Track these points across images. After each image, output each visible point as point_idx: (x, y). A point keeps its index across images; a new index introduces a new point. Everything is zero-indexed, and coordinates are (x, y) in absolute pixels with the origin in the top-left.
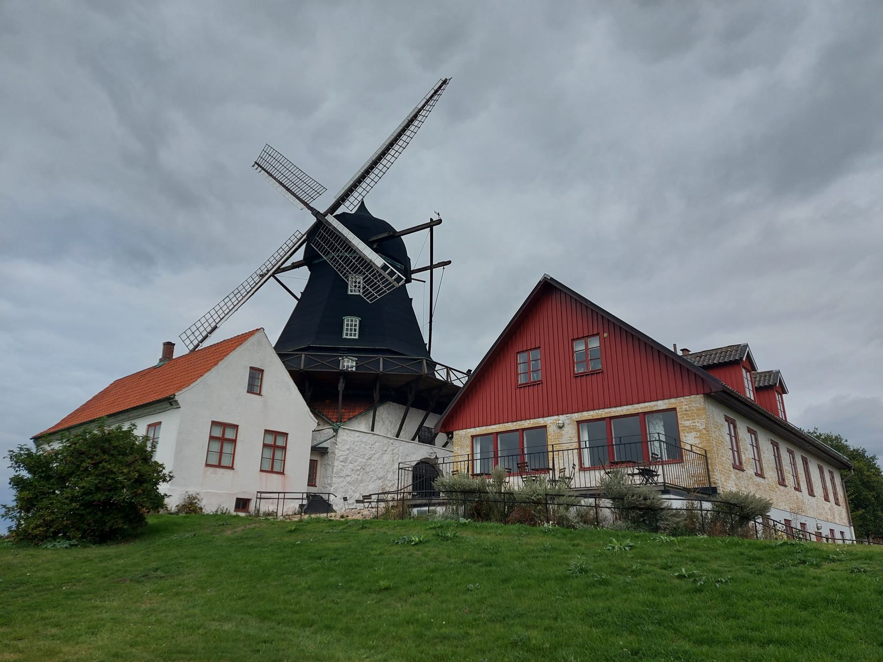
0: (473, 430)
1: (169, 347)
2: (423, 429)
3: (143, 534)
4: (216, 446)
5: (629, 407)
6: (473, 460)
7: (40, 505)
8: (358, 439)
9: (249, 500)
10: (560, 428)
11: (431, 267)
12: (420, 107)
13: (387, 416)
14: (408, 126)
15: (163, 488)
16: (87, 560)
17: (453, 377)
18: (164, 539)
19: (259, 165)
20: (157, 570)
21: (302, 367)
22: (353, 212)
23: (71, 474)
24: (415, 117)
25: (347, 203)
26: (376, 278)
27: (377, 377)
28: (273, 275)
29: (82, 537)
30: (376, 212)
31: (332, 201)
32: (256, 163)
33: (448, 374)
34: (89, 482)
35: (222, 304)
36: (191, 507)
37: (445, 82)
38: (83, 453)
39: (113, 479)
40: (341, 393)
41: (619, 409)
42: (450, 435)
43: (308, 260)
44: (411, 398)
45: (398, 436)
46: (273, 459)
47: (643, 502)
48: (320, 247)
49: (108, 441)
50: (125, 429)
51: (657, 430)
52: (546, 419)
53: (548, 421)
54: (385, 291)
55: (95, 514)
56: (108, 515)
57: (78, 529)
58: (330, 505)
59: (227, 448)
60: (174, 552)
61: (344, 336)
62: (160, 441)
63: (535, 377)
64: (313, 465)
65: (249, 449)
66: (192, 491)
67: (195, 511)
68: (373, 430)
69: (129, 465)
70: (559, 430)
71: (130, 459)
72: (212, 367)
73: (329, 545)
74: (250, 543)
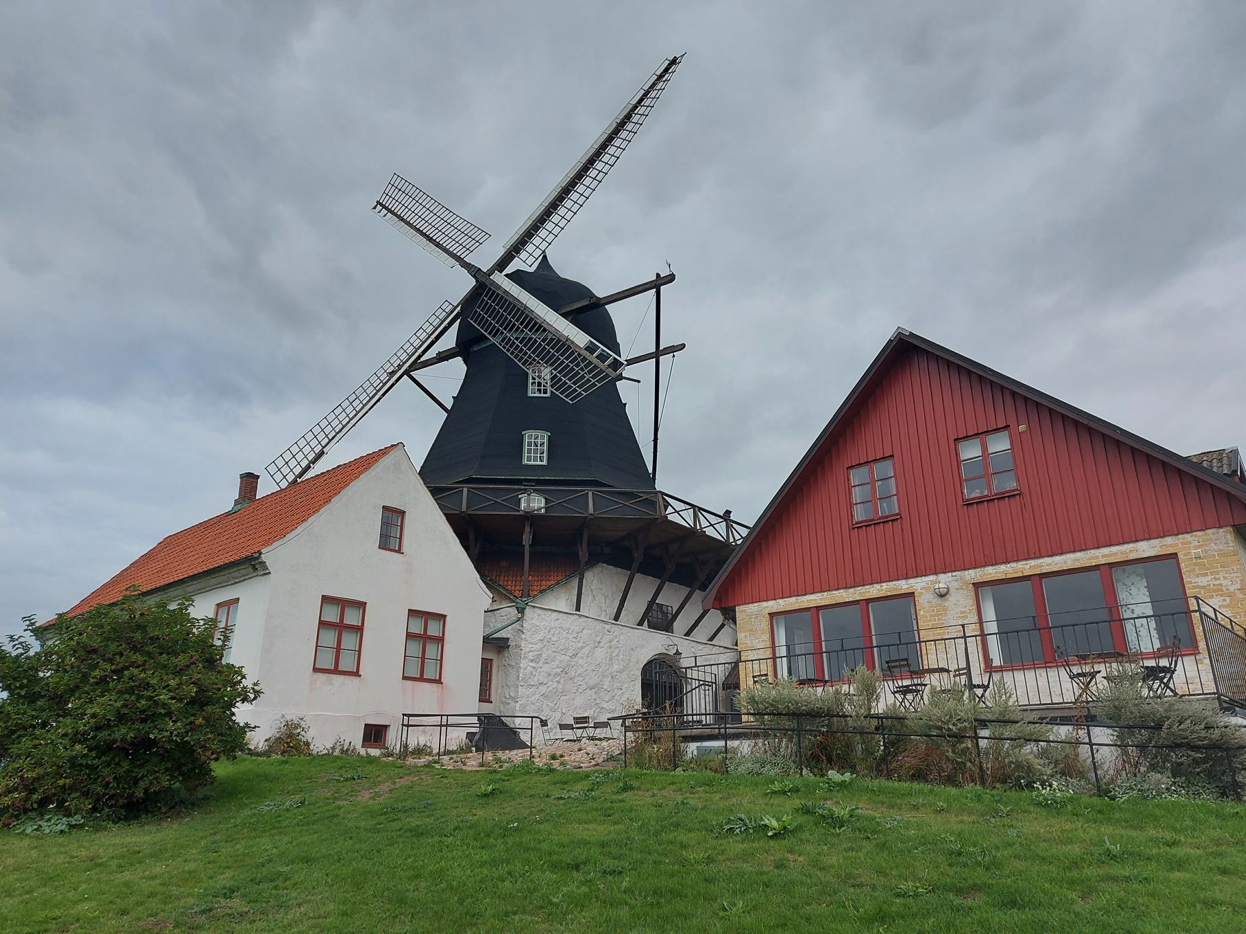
0: (771, 603)
1: (249, 480)
2: (655, 607)
3: (206, 798)
4: (330, 638)
5: (1078, 555)
6: (774, 658)
7: (14, 749)
8: (557, 624)
9: (386, 727)
10: (942, 596)
11: (657, 354)
12: (634, 102)
13: (601, 586)
14: (616, 131)
15: (242, 714)
16: (95, 862)
17: (704, 523)
18: (247, 812)
19: (384, 207)
20: (229, 893)
21: (464, 508)
22: (532, 270)
23: (72, 691)
24: (628, 117)
25: (523, 255)
26: (577, 365)
27: (584, 522)
28: (407, 373)
29: (95, 809)
30: (566, 268)
31: (500, 252)
32: (378, 203)
33: (695, 516)
34: (103, 705)
35: (332, 416)
36: (290, 742)
37: (674, 62)
38: (94, 651)
39: (150, 698)
40: (527, 549)
41: (1058, 559)
42: (730, 615)
43: (464, 348)
44: (638, 556)
45: (617, 618)
46: (423, 658)
47: (1203, 733)
48: (485, 327)
49: (141, 627)
50: (173, 606)
51: (1136, 599)
52: (912, 581)
53: (917, 584)
54: (580, 394)
55: (118, 764)
56: (142, 766)
57: (86, 794)
58: (514, 732)
59: (349, 640)
60: (265, 843)
61: (525, 462)
62: (236, 629)
63: (884, 509)
64: (486, 666)
65: (385, 641)
66: (292, 714)
67: (296, 748)
68: (578, 609)
69: (179, 672)
70: (939, 601)
71: (181, 660)
72: (321, 507)
73: (580, 832)
74: (414, 821)
